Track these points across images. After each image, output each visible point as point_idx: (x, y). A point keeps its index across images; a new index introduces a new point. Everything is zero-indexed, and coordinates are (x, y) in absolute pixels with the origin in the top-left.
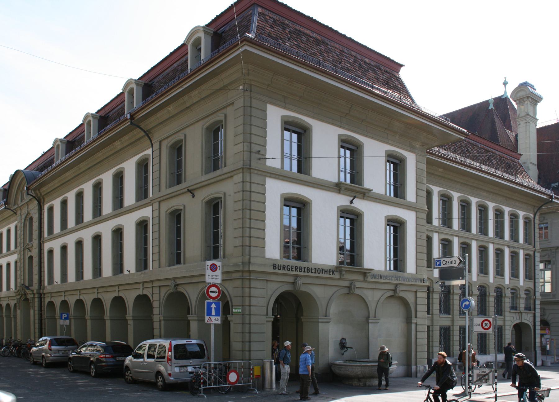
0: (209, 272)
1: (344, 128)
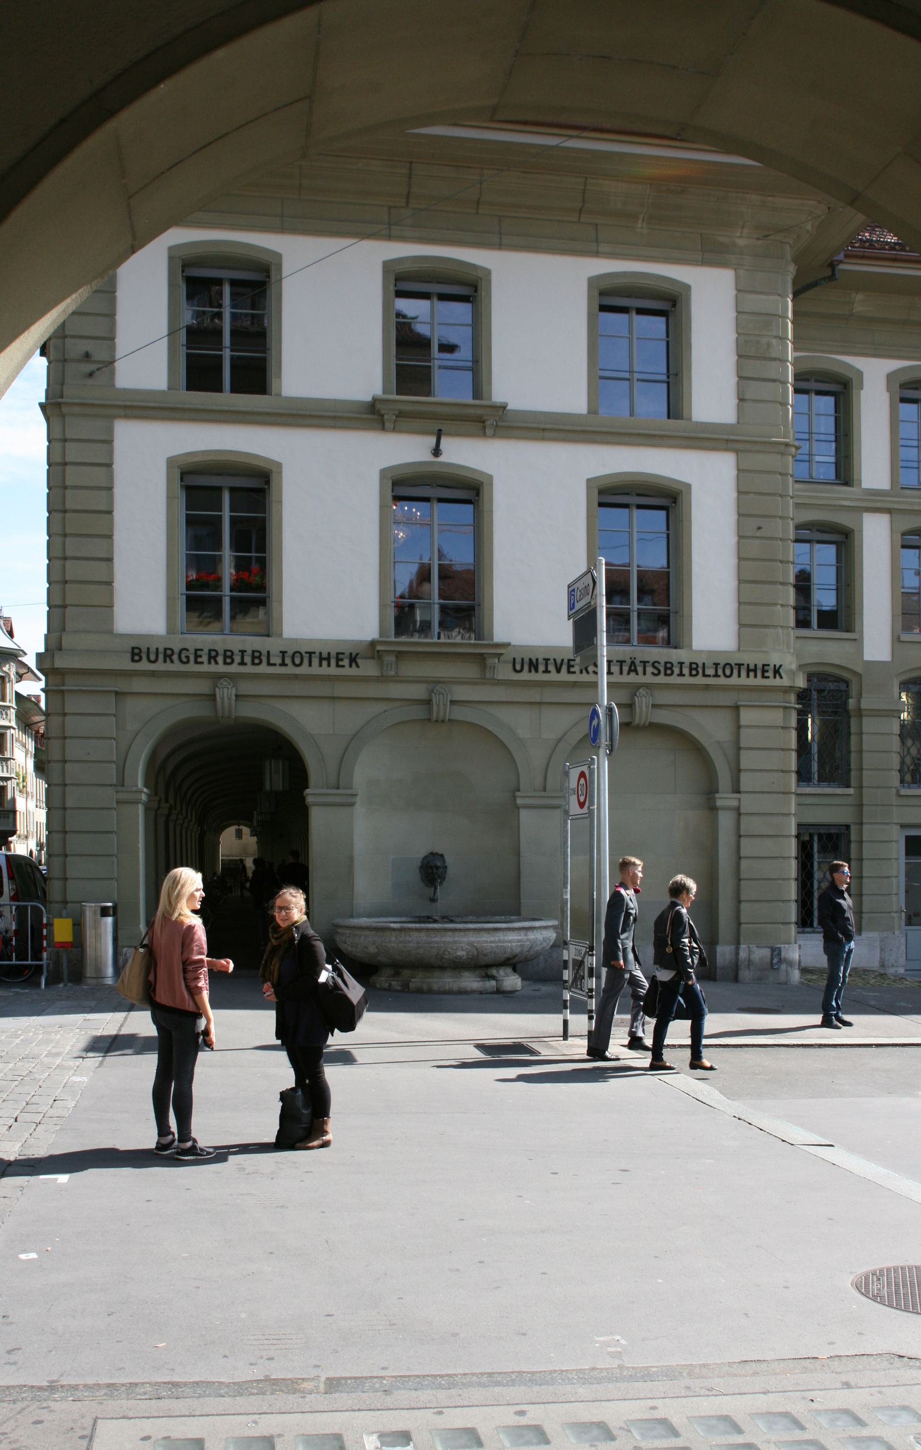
1: (403, 239)
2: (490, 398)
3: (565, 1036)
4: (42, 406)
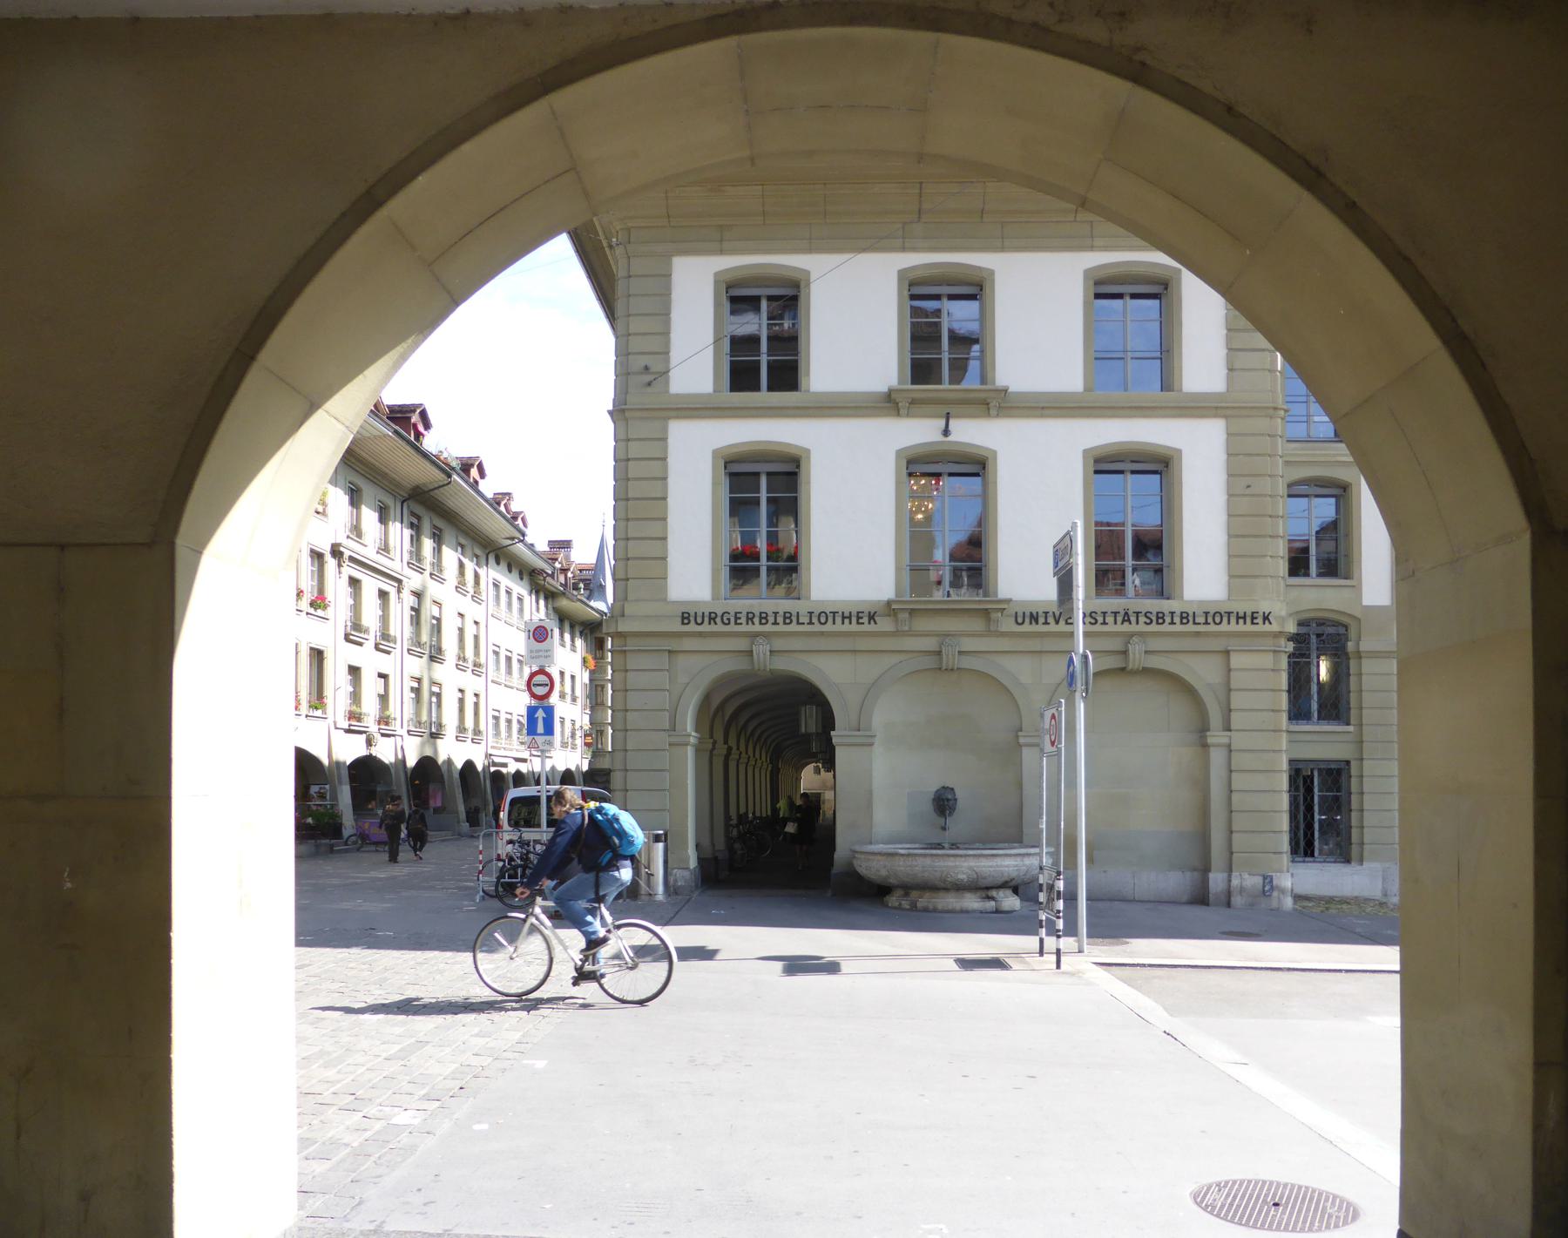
1: (914, 249)
2: (994, 382)
3: (1041, 953)
4: (610, 413)
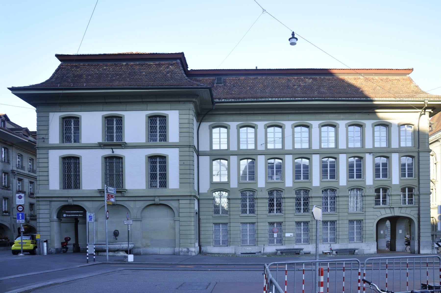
0: (18, 199)
